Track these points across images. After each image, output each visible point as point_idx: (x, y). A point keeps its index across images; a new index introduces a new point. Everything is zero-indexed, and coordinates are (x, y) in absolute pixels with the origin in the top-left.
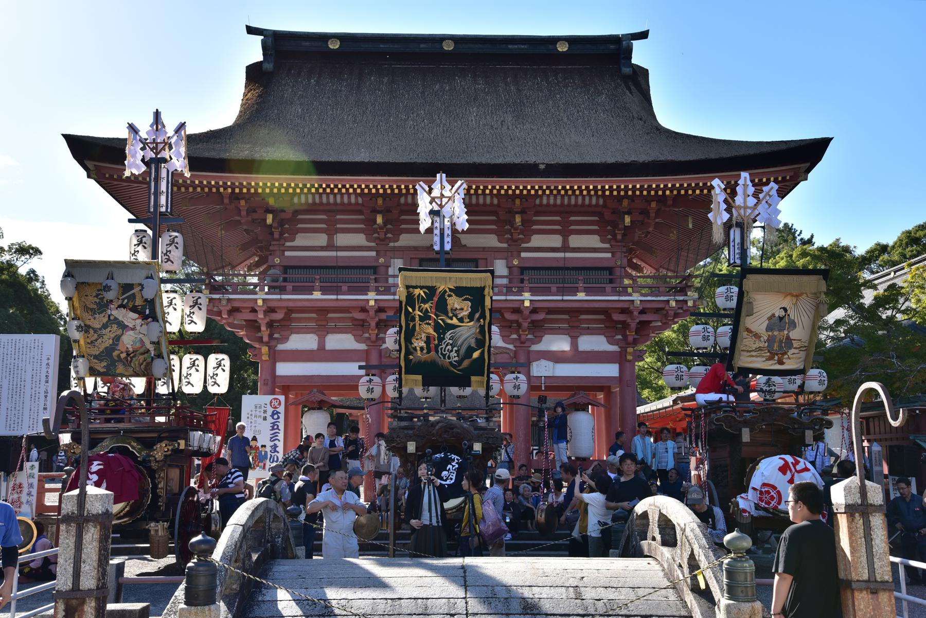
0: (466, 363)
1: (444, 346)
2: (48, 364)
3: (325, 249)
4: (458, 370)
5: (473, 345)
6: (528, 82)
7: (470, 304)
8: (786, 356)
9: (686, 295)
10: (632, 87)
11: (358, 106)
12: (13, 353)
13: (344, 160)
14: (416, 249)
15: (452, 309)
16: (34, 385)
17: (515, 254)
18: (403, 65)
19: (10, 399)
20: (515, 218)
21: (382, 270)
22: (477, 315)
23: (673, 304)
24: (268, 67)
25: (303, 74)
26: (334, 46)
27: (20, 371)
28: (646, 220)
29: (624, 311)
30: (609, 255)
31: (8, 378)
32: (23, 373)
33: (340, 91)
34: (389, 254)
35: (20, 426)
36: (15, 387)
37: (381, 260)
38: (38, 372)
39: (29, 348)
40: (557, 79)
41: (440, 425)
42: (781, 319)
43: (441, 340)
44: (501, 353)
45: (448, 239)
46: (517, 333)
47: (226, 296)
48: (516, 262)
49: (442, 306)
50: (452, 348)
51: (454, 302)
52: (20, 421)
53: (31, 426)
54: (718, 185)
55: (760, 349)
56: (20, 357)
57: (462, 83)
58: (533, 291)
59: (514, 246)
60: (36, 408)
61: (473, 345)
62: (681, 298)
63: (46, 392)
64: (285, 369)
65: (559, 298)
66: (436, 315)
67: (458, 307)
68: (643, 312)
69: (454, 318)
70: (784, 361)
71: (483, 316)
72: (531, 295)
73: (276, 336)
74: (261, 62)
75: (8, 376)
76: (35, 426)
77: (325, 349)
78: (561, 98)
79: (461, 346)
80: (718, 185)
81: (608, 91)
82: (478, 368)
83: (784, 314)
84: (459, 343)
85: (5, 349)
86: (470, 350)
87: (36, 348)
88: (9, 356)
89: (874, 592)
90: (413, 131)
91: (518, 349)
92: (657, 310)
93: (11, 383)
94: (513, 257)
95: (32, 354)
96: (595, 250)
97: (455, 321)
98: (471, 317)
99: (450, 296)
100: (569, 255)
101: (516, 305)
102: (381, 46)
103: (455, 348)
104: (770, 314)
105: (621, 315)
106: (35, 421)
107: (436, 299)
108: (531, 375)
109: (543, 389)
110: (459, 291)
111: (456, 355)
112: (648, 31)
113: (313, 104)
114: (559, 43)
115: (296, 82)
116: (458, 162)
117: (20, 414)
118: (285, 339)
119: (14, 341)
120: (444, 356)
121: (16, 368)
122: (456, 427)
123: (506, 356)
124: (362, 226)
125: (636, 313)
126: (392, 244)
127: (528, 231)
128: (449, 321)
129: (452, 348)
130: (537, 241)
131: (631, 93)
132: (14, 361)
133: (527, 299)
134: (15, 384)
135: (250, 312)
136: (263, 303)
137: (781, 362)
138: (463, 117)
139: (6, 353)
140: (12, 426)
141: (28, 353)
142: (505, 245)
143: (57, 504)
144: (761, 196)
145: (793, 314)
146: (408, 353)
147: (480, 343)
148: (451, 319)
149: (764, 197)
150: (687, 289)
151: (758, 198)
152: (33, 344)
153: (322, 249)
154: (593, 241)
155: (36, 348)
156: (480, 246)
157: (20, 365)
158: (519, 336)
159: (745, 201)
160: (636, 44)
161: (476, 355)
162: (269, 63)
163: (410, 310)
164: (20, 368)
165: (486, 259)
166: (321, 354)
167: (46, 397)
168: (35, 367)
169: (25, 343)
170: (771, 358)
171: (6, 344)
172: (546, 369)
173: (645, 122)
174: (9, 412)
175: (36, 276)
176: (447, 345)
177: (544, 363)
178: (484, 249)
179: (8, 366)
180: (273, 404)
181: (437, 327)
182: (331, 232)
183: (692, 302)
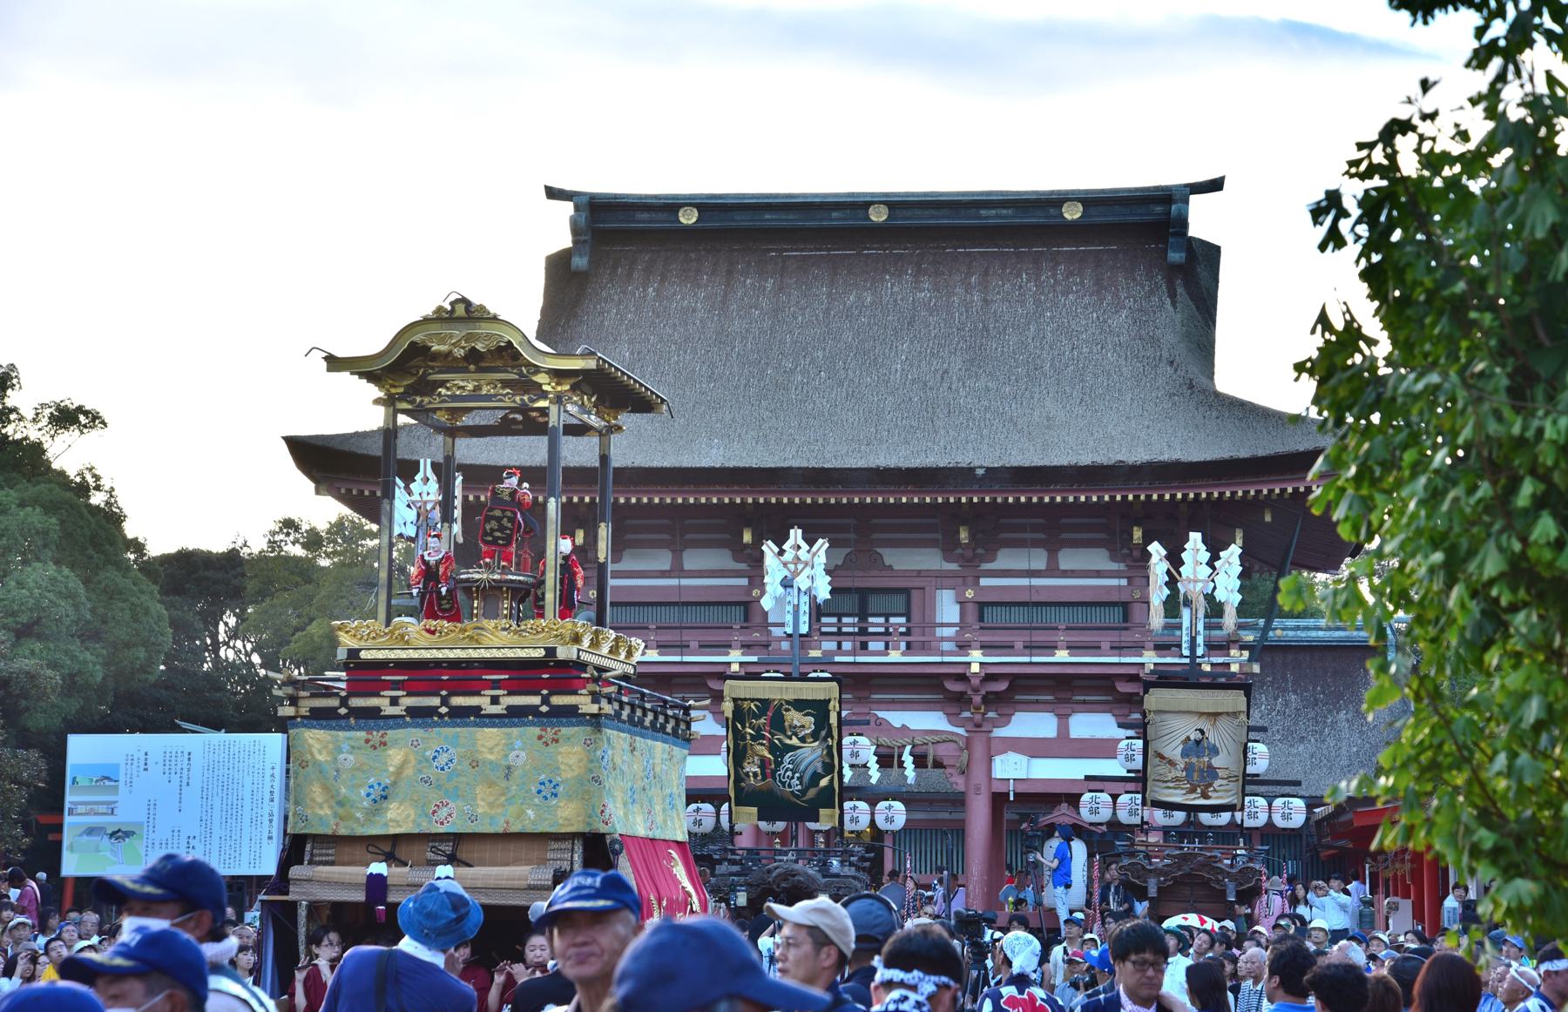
0: (812, 793)
1: (782, 772)
2: (273, 775)
3: (667, 574)
4: (802, 801)
5: (820, 770)
6: (1003, 285)
7: (813, 720)
8: (1212, 789)
9: (1228, 655)
10: (1180, 290)
11: (720, 342)
12: (226, 760)
13: (685, 465)
15: (790, 726)
16: (255, 805)
17: (970, 580)
18: (802, 250)
19: (224, 824)
20: (958, 532)
22: (823, 733)
25: (636, 275)
26: (689, 219)
27: (235, 785)
30: (1124, 582)
31: (220, 795)
32: (240, 788)
33: (694, 311)
35: (237, 862)
36: (229, 807)
38: (260, 786)
39: (247, 753)
40: (1054, 276)
41: (778, 871)
42: (1198, 742)
43: (779, 764)
44: (944, 741)
45: (804, 619)
48: (970, 594)
49: (778, 724)
50: (793, 774)
51: (794, 717)
52: (237, 855)
53: (252, 862)
54: (1157, 551)
55: (1177, 779)
56: (236, 766)
57: (895, 289)
60: (258, 838)
61: (820, 771)
62: (1220, 660)
63: (271, 815)
65: (1026, 659)
66: (770, 733)
67: (798, 725)
69: (794, 737)
70: (1210, 794)
71: (830, 734)
72: (984, 655)
75: (220, 792)
76: (257, 862)
78: (1052, 318)
79: (804, 772)
80: (1157, 551)
81: (1135, 301)
82: (827, 798)
83: (1201, 737)
84: (802, 767)
85: (216, 755)
86: (816, 777)
87: (257, 753)
88: (221, 764)
90: (799, 397)
91: (972, 734)
93: (224, 803)
94: (965, 586)
95: (252, 760)
97: (795, 741)
98: (815, 736)
99: (787, 710)
101: (959, 670)
102: (767, 216)
103: (797, 775)
104: (1184, 737)
105: (1130, 684)
106: (258, 854)
107: (770, 714)
109: (1012, 799)
110: (799, 705)
111: (798, 782)
112: (1222, 179)
113: (649, 340)
114: (1066, 205)
115: (624, 292)
116: (854, 466)
117: (238, 846)
119: (227, 743)
120: (783, 784)
121: (230, 781)
122: (799, 874)
123: (952, 745)
128: (788, 741)
129: (793, 774)
131: (1174, 304)
132: (227, 771)
133: (976, 658)
134: (230, 804)
137: (1205, 796)
138: (882, 365)
139: (216, 760)
140: (227, 862)
141: (246, 760)
142: (954, 566)
144: (1217, 564)
145: (1212, 737)
146: (738, 780)
147: (828, 768)
148: (790, 738)
149: (1223, 565)
151: (1214, 568)
152: (252, 747)
153: (663, 574)
155: (257, 753)
157: (236, 776)
159: (1195, 572)
161: (824, 782)
162: (581, 256)
163: (739, 726)
164: (236, 781)
165: (924, 588)
167: (271, 821)
168: (255, 779)
169: (242, 746)
170: (1192, 790)
171: (217, 747)
172: (1016, 766)
173: (1176, 370)
174: (223, 842)
175: (97, 478)
176: (787, 771)
177: (1012, 757)
178: (919, 573)
179: (221, 778)
181: (772, 748)
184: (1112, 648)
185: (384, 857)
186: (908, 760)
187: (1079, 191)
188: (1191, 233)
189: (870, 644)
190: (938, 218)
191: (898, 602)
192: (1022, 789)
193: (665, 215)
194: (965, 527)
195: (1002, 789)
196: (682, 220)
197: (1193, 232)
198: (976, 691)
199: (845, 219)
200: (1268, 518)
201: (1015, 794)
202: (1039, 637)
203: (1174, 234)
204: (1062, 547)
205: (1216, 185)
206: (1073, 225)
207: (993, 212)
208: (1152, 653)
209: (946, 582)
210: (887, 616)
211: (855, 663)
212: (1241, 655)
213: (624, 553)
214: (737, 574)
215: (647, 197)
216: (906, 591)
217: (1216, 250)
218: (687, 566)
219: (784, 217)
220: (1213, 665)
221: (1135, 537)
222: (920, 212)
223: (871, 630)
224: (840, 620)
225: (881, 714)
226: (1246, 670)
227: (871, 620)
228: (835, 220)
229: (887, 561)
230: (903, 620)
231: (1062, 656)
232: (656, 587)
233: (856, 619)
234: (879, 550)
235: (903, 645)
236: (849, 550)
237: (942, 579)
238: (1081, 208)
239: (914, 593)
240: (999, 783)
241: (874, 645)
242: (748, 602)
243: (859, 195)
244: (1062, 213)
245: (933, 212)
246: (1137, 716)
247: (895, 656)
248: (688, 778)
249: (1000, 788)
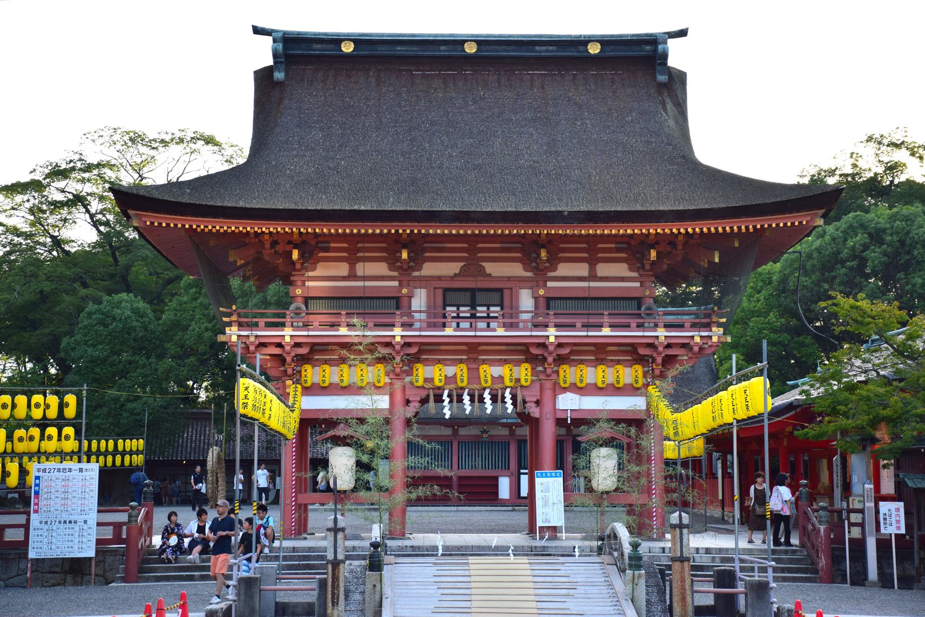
14: (439, 278)
17: (541, 283)
21: (404, 302)
23: (697, 339)
24: (280, 77)
28: (674, 252)
29: (651, 346)
30: (638, 284)
34: (411, 283)
37: (405, 291)
46: (543, 365)
47: (255, 333)
48: (542, 292)
58: (558, 326)
59: (540, 274)
62: (706, 334)
65: (584, 334)
68: (669, 346)
72: (557, 331)
74: (271, 67)
89: (682, 562)
92: (684, 346)
96: (622, 279)
100: (592, 284)
102: (399, 48)
109: (569, 422)
114: (590, 44)
124: (384, 254)
125: (661, 349)
126: (416, 274)
127: (554, 262)
130: (564, 269)
133: (552, 334)
142: (529, 274)
143: (22, 539)
150: (712, 325)
153: (344, 278)
156: (502, 275)
158: (545, 369)
160: (672, 43)
162: (280, 72)
165: (511, 289)
183: (717, 337)
184: (583, 326)
186: (487, 396)
187: (598, 36)
188: (272, 63)
189: (491, 324)
190: (508, 51)
191: (496, 296)
193: (332, 46)
194: (545, 250)
195: (562, 416)
196: (343, 49)
197: (669, 64)
198: (550, 353)
199: (448, 51)
200: (737, 245)
201: (571, 419)
202: (592, 320)
203: (659, 64)
204: (358, 261)
205: (683, 33)
206: (347, 56)
207: (544, 48)
208: (663, 329)
209: (522, 284)
210: (488, 306)
211: (475, 336)
213: (318, 265)
214: (392, 278)
215: (319, 34)
216: (500, 290)
217: (255, 72)
218: (360, 273)
219: (409, 49)
220: (702, 337)
221: (652, 256)
222: (497, 47)
223: (478, 315)
224: (458, 309)
226: (723, 340)
227: (479, 308)
228: (443, 51)
229: (488, 271)
230: (498, 309)
232: (352, 287)
233: (469, 308)
234: (483, 264)
235: (454, 324)
236: (463, 264)
238: (599, 46)
239: (507, 294)
240: (560, 412)
241: (482, 325)
242: (399, 297)
243: (457, 35)
244: (587, 50)
245: (505, 47)
247: (501, 332)
248: (303, 411)
249: (560, 415)
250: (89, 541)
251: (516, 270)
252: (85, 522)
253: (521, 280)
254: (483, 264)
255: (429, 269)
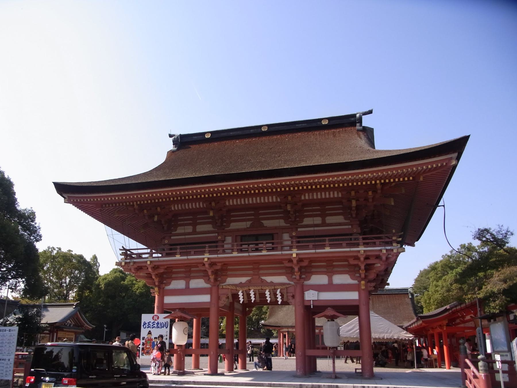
14: (238, 230)
23: (384, 251)
30: (350, 227)
37: (219, 238)
48: (294, 234)
64: (169, 300)
73: (303, 276)
77: (189, 288)
108: (305, 299)
109: (312, 307)
114: (323, 121)
118: (169, 284)
130: (307, 221)
135: (288, 262)
136: (296, 255)
142: (216, 229)
153: (189, 234)
154: (340, 219)
165: (278, 233)
166: (330, 287)
172: (313, 295)
180: (154, 318)
182: (194, 225)
183: (396, 249)
185: (347, 377)
192: (317, 304)
201: (313, 306)
205: (370, 112)
206: (325, 125)
212: (397, 246)
217: (373, 129)
220: (387, 250)
225: (263, 278)
231: (328, 249)
234: (262, 221)
236: (251, 222)
237: (283, 229)
246: (358, 275)
249: (307, 304)
250: (10, 370)
251: (281, 223)
252: (9, 360)
253: (283, 229)
254: (262, 221)
255: (234, 226)
